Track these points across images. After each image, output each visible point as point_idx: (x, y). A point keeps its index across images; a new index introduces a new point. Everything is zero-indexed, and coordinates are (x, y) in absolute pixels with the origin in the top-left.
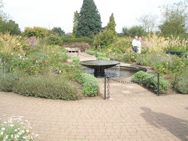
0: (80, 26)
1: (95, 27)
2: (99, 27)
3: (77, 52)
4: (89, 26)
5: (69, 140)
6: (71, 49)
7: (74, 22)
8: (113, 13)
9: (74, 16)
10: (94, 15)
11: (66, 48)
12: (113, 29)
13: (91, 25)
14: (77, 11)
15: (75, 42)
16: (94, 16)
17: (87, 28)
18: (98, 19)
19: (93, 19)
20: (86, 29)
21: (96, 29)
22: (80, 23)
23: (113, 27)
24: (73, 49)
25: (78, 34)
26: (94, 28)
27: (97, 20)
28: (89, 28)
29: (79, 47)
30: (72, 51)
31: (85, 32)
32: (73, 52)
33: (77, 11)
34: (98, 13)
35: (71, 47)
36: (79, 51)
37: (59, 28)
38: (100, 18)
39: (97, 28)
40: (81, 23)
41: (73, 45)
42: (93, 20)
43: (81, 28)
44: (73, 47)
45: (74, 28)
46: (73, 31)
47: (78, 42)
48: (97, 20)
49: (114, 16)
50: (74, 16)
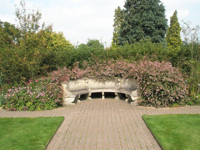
0: (125, 28)
1: (154, 29)
2: (162, 27)
3: (123, 96)
4: (143, 26)
5: (116, 149)
6: (101, 84)
7: (114, 26)
8: (176, 11)
9: (115, 16)
10: (152, 5)
11: (7, 136)
12: (177, 36)
13: (147, 23)
14: (119, 7)
15: (115, 58)
16: (153, 7)
17: (139, 30)
18: (160, 13)
19: (151, 12)
20: (138, 31)
21: (158, 31)
22: (127, 22)
23: (177, 33)
24: (110, 86)
25: (121, 43)
26: (154, 31)
27: (158, 15)
28: (144, 30)
29: (131, 77)
30: (103, 91)
31: (135, 38)
32: (109, 95)
33: (119, 7)
34: (160, 4)
35: (102, 78)
36: (134, 96)
37: (96, 40)
38: (163, 11)
39: (159, 29)
40: (128, 22)
41: (109, 70)
42: (151, 15)
43: (128, 30)
44: (109, 78)
45: (114, 34)
46: (114, 39)
47: (125, 57)
48: (158, 15)
49: (178, 16)
50: (115, 16)
